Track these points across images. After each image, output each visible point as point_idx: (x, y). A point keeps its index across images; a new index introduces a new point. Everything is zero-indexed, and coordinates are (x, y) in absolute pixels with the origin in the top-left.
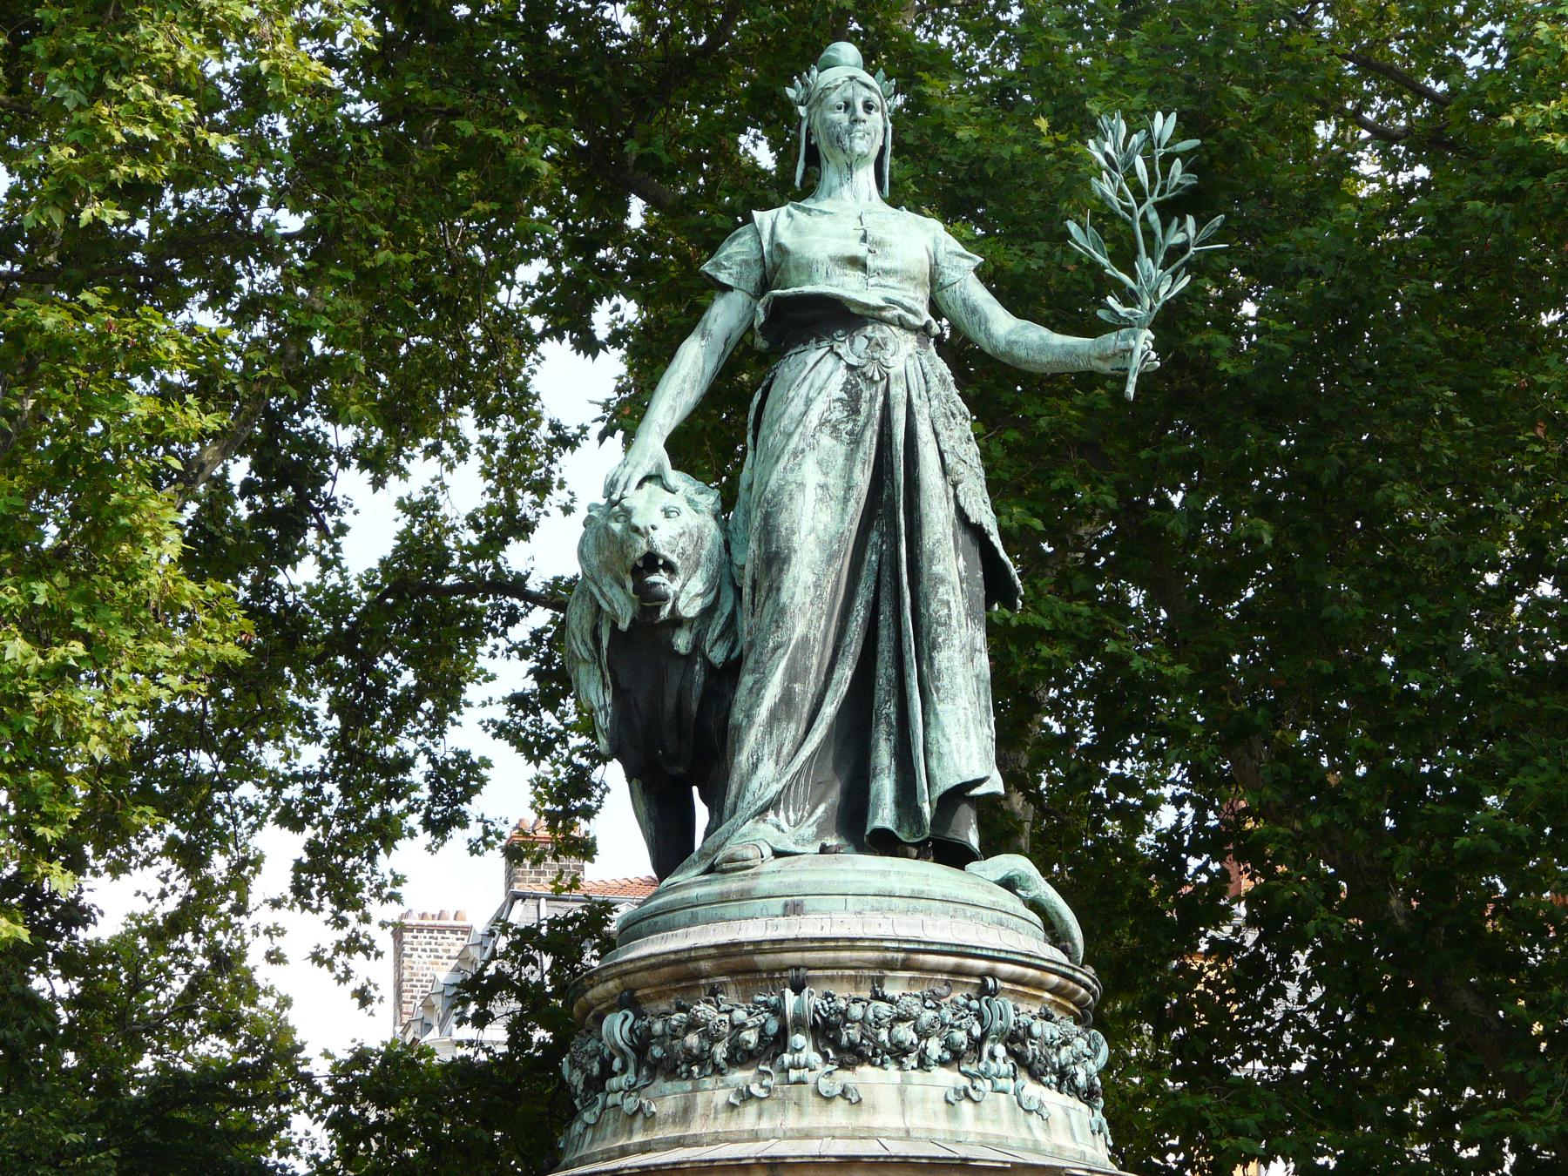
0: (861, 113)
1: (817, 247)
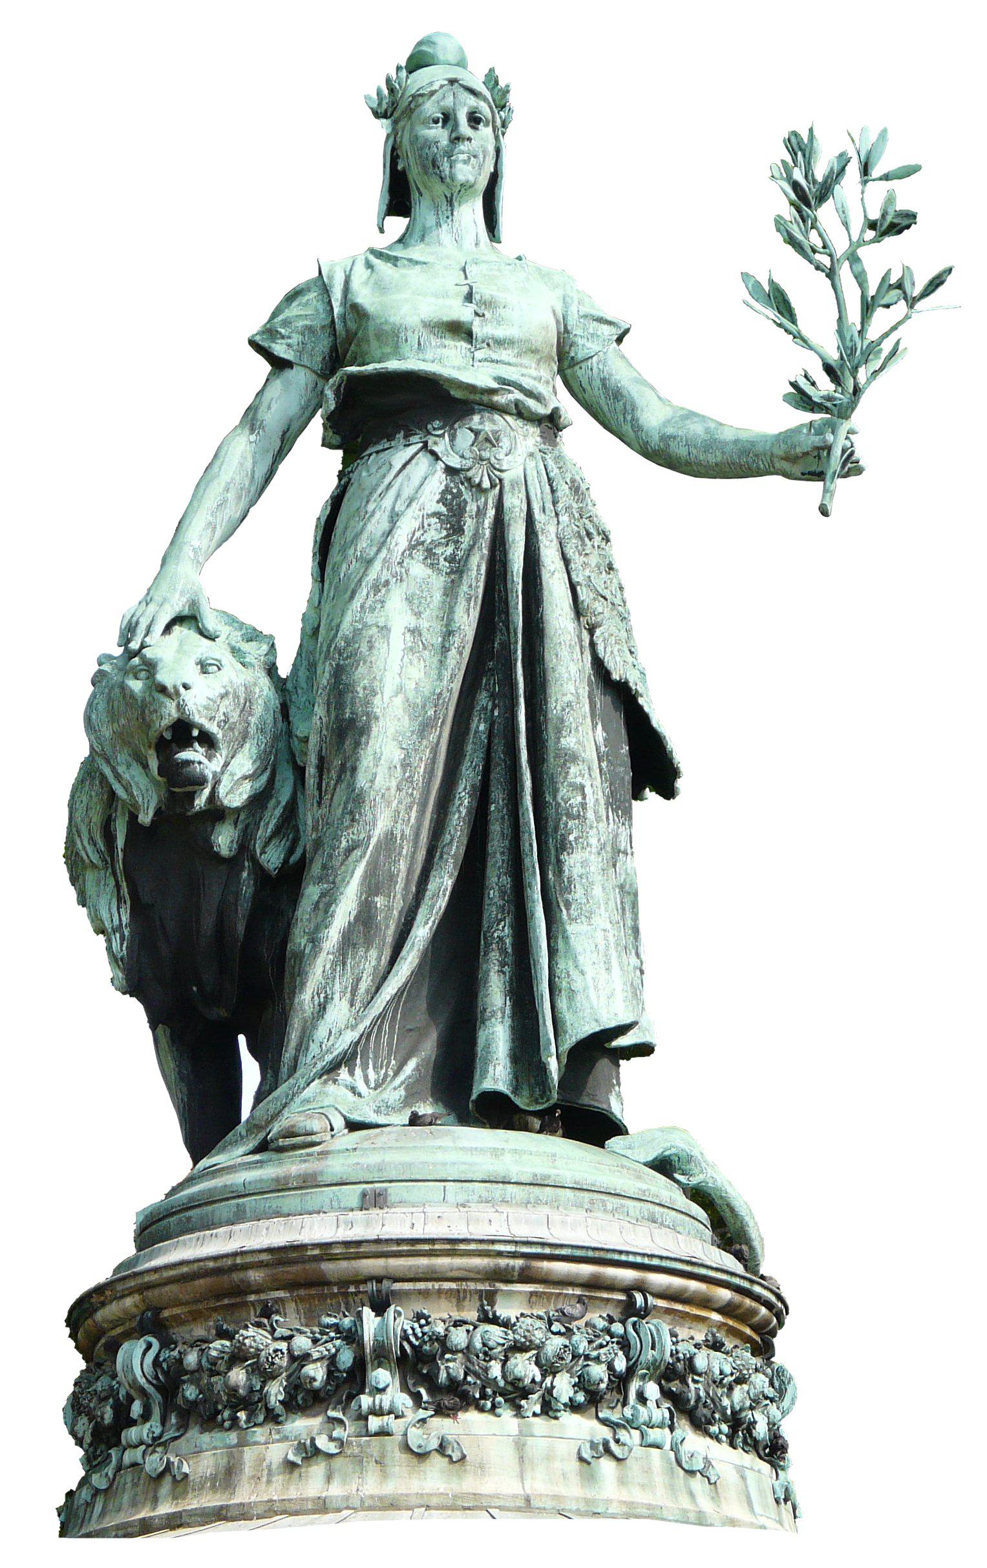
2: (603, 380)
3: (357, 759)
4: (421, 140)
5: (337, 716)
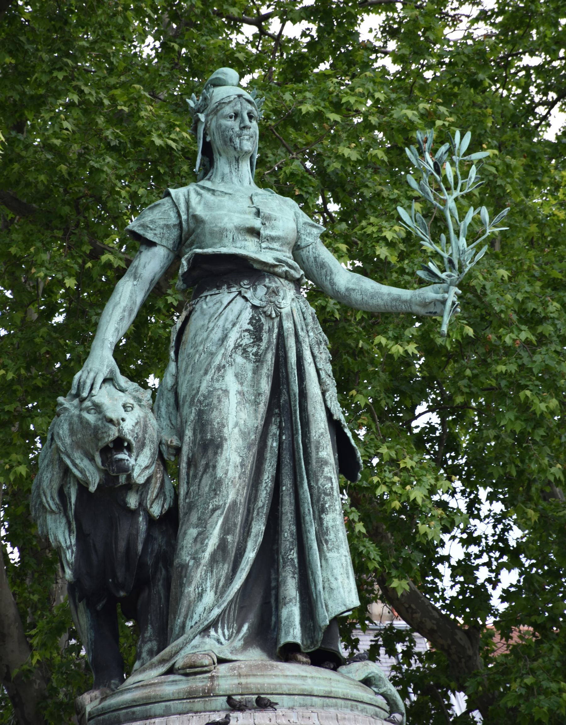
0: (247, 122)
1: (226, 219)
2: (315, 258)
3: (216, 461)
4: (224, 127)
5: (202, 438)
